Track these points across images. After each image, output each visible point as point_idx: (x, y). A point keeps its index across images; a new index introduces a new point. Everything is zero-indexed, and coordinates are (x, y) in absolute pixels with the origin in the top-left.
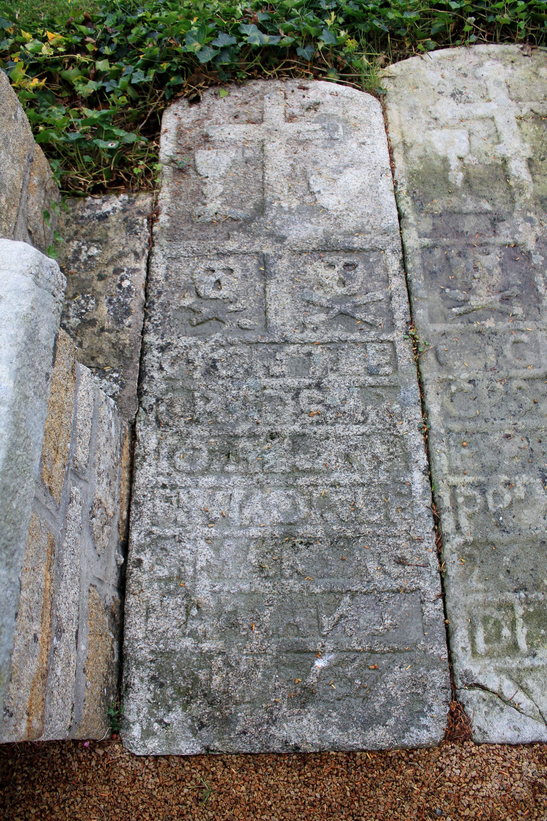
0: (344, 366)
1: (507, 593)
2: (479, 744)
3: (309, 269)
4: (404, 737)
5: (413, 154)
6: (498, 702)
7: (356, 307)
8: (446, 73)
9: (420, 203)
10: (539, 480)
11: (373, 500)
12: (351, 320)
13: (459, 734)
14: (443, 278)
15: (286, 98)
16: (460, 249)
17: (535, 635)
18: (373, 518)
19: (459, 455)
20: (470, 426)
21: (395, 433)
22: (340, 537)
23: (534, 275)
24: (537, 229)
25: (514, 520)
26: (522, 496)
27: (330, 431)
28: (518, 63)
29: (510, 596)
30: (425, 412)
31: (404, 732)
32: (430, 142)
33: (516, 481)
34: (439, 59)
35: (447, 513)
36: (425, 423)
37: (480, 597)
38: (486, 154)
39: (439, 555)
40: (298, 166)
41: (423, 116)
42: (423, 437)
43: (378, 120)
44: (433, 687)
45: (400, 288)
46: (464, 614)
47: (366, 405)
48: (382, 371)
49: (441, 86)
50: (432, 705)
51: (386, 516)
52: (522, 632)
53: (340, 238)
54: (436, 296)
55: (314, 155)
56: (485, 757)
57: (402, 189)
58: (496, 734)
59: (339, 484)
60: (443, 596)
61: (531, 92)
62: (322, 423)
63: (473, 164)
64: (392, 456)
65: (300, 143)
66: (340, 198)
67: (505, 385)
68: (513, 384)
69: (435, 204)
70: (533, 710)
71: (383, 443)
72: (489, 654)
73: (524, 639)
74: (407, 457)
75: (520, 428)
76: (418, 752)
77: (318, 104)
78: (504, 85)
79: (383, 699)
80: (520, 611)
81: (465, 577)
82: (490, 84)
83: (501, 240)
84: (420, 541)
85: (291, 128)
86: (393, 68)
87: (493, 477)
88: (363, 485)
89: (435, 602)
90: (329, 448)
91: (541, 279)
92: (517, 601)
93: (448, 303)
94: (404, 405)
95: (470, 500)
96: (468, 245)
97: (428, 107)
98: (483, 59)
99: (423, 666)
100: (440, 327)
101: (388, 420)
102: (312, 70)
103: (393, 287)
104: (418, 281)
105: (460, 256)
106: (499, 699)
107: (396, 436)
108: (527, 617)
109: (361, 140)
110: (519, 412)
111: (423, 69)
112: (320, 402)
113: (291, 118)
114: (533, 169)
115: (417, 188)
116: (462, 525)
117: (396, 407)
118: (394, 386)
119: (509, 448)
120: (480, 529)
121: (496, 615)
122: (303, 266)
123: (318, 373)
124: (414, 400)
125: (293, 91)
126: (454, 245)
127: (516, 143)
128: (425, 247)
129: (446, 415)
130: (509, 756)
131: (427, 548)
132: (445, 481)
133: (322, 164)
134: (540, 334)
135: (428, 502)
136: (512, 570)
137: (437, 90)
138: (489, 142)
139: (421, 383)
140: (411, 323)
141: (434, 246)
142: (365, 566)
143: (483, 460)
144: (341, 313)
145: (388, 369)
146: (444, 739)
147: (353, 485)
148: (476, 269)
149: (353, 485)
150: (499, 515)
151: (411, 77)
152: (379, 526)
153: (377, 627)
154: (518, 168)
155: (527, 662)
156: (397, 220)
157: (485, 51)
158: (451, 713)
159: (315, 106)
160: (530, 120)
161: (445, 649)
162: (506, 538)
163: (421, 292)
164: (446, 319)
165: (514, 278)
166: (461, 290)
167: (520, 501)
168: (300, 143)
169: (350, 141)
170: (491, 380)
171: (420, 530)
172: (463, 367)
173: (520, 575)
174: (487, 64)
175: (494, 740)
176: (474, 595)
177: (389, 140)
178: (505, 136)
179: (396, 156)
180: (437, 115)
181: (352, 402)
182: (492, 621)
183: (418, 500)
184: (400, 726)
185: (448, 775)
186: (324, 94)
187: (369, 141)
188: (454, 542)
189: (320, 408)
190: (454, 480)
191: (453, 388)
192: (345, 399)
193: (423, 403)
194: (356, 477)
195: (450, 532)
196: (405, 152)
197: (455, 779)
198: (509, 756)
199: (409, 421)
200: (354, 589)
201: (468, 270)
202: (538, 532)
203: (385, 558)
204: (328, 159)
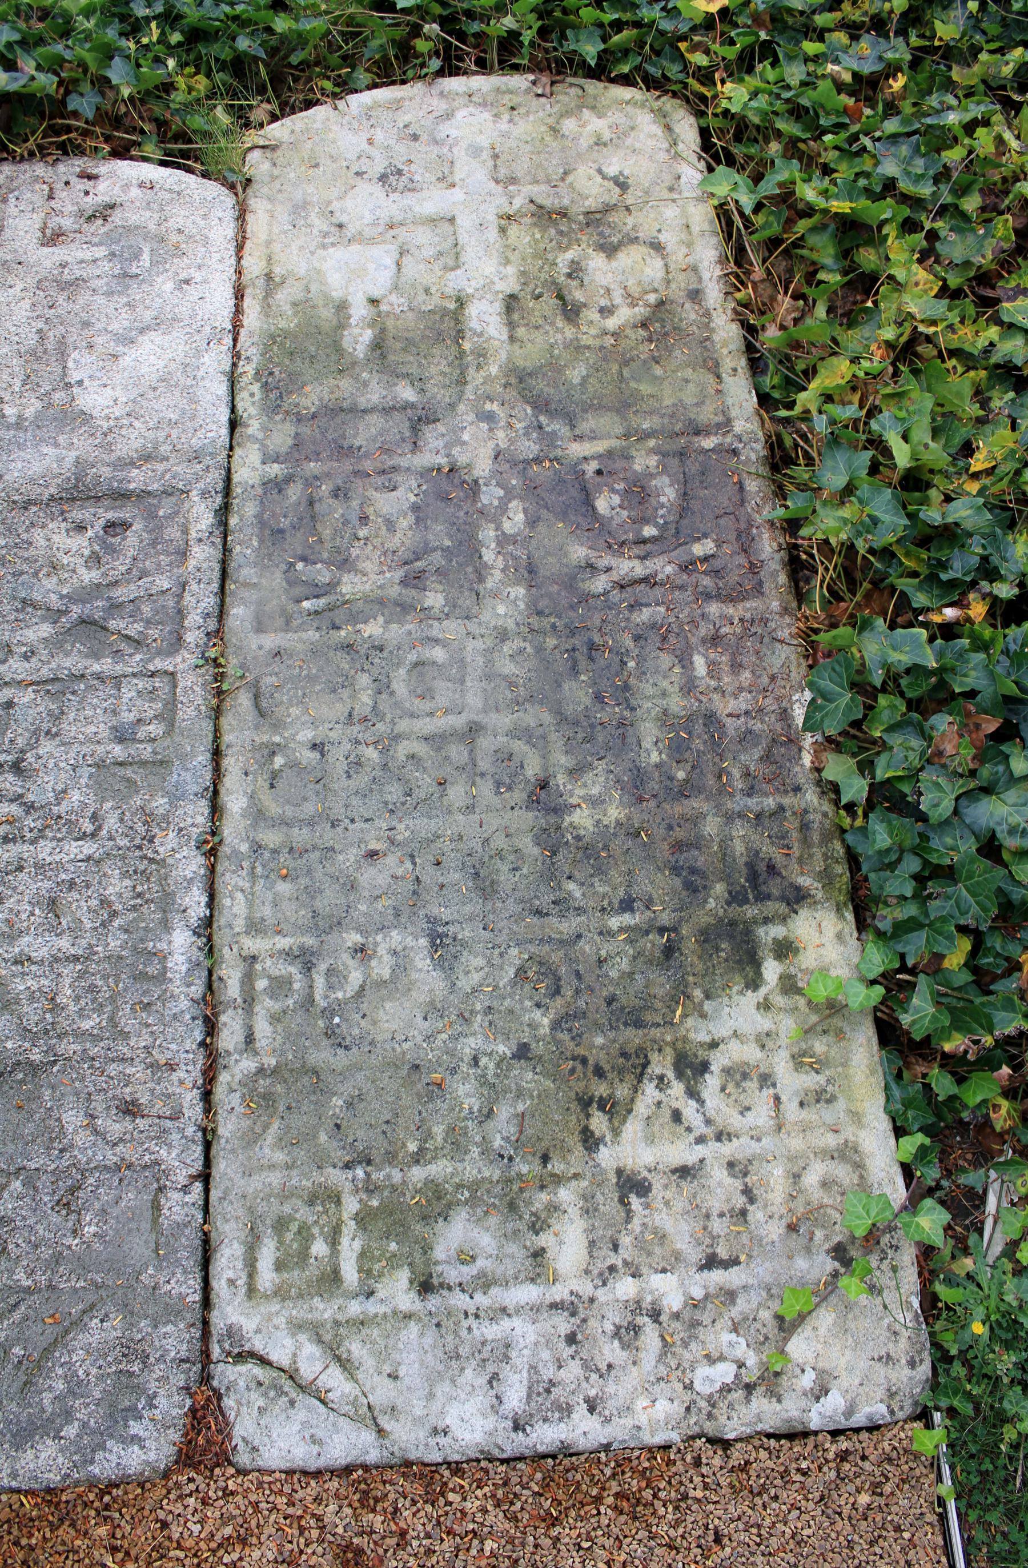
0: (69, 728)
1: (331, 1170)
2: (245, 1473)
3: (38, 536)
4: (92, 1462)
5: (283, 297)
6: (286, 1389)
7: (115, 607)
8: (379, 135)
9: (276, 392)
10: (423, 942)
11: (92, 989)
12: (101, 635)
13: (205, 1452)
14: (295, 543)
15: (51, 197)
16: (340, 482)
17: (377, 1253)
18: (86, 1025)
19: (269, 896)
20: (300, 836)
21: (150, 855)
22: (19, 1063)
23: (478, 527)
24: (501, 434)
25: (363, 1023)
26: (386, 973)
27: (26, 855)
28: (522, 111)
29: (336, 1177)
30: (216, 809)
31: (93, 1451)
32: (318, 272)
33: (376, 944)
34: (370, 108)
35: (230, 1012)
36: (213, 834)
37: (275, 1179)
38: (427, 291)
39: (207, 1096)
40: (51, 334)
41: (317, 222)
42: (201, 860)
43: (224, 231)
44: (161, 1359)
45: (205, 565)
46: (240, 1212)
47: (103, 800)
48: (142, 733)
49: (364, 160)
50: (155, 1395)
51: (111, 1019)
52: (350, 1248)
53: (106, 472)
54: (277, 579)
55: (87, 308)
56: (253, 1497)
57: (247, 368)
58: (275, 1452)
59: (29, 959)
60: (205, 1177)
61: (539, 165)
62: (14, 840)
63: (398, 310)
64: (139, 901)
65: (64, 286)
66: (118, 393)
67: (384, 751)
68: (400, 748)
69: (306, 396)
70: (354, 1403)
71: (125, 875)
72: (280, 1293)
73: (353, 1261)
74: (167, 902)
75: (400, 837)
76: (120, 1492)
77: (112, 207)
78: (486, 155)
79: (60, 1386)
80: (351, 1205)
81: (251, 1139)
82: (460, 153)
83: (426, 459)
84: (171, 1067)
85: (49, 258)
86: (277, 131)
87: (332, 939)
88: (76, 958)
89: (185, 1189)
90: (21, 888)
91: (492, 533)
92: (349, 1186)
93: (298, 591)
94: (175, 798)
95: (280, 986)
96: (356, 473)
97: (329, 203)
98: (456, 104)
99: (146, 1317)
100: (270, 641)
101: (140, 828)
102: (108, 139)
103: (192, 563)
104: (244, 551)
105: (336, 496)
106: (289, 1382)
107: (152, 860)
108: (362, 1219)
109: (183, 275)
110: (403, 804)
111: (334, 128)
112: (18, 798)
113: (52, 238)
114: (516, 316)
115: (278, 365)
116: (257, 1035)
117: (160, 803)
118: (162, 762)
119: (372, 877)
120: (294, 1044)
121: (304, 1214)
122: (27, 531)
123: (20, 742)
124: (195, 788)
125: (67, 183)
126: (328, 475)
127: (489, 267)
128: (270, 481)
129: (257, 815)
130: (301, 1494)
131: (181, 1082)
132: (235, 948)
133: (99, 326)
134: (471, 645)
135: (197, 990)
136: (344, 1124)
137: (355, 168)
138: (437, 267)
139: (217, 754)
140: (217, 634)
141: (289, 479)
142: (59, 1120)
143: (318, 904)
144: (83, 621)
145: (155, 729)
146: (176, 1462)
147: (57, 960)
148: (364, 519)
149: (57, 960)
150: (333, 1014)
151: (309, 145)
152: (96, 1039)
153: (69, 1241)
154: (485, 318)
155: (355, 1308)
156: (224, 431)
157: (462, 89)
158: (193, 1411)
159: (104, 212)
160: (528, 220)
161: (195, 1283)
162: (341, 1059)
163: (244, 571)
164: (288, 622)
165: (440, 535)
166: (327, 563)
167: (382, 983)
168: (64, 286)
169: (159, 280)
170: (358, 742)
171: (173, 1047)
172: (306, 717)
173: (361, 1134)
174: (460, 114)
175: (273, 1464)
176: (265, 1174)
177: (239, 272)
178: (469, 256)
179: (247, 302)
180: (344, 219)
181: (76, 796)
182: (294, 1227)
183: (176, 987)
184: (86, 1440)
185: (176, 1536)
186: (126, 187)
187: (198, 277)
188: (237, 1070)
189: (15, 809)
190: (252, 945)
191: (279, 761)
192: (64, 791)
193: (216, 793)
194: (64, 943)
195: (231, 1049)
196: (268, 294)
197: (189, 1543)
198: (301, 1494)
199: (181, 830)
200: (33, 1165)
201: (346, 522)
202: (406, 1046)
203: (98, 1105)
204: (112, 315)
